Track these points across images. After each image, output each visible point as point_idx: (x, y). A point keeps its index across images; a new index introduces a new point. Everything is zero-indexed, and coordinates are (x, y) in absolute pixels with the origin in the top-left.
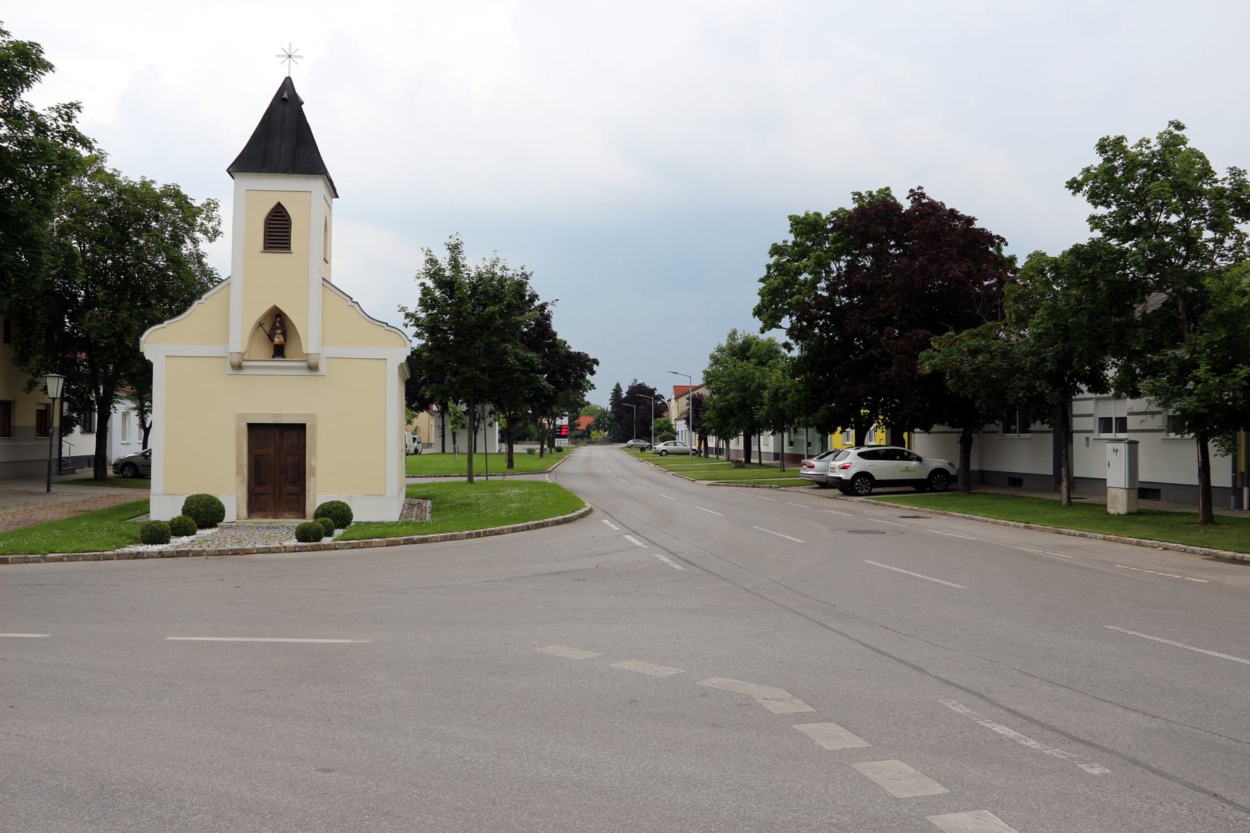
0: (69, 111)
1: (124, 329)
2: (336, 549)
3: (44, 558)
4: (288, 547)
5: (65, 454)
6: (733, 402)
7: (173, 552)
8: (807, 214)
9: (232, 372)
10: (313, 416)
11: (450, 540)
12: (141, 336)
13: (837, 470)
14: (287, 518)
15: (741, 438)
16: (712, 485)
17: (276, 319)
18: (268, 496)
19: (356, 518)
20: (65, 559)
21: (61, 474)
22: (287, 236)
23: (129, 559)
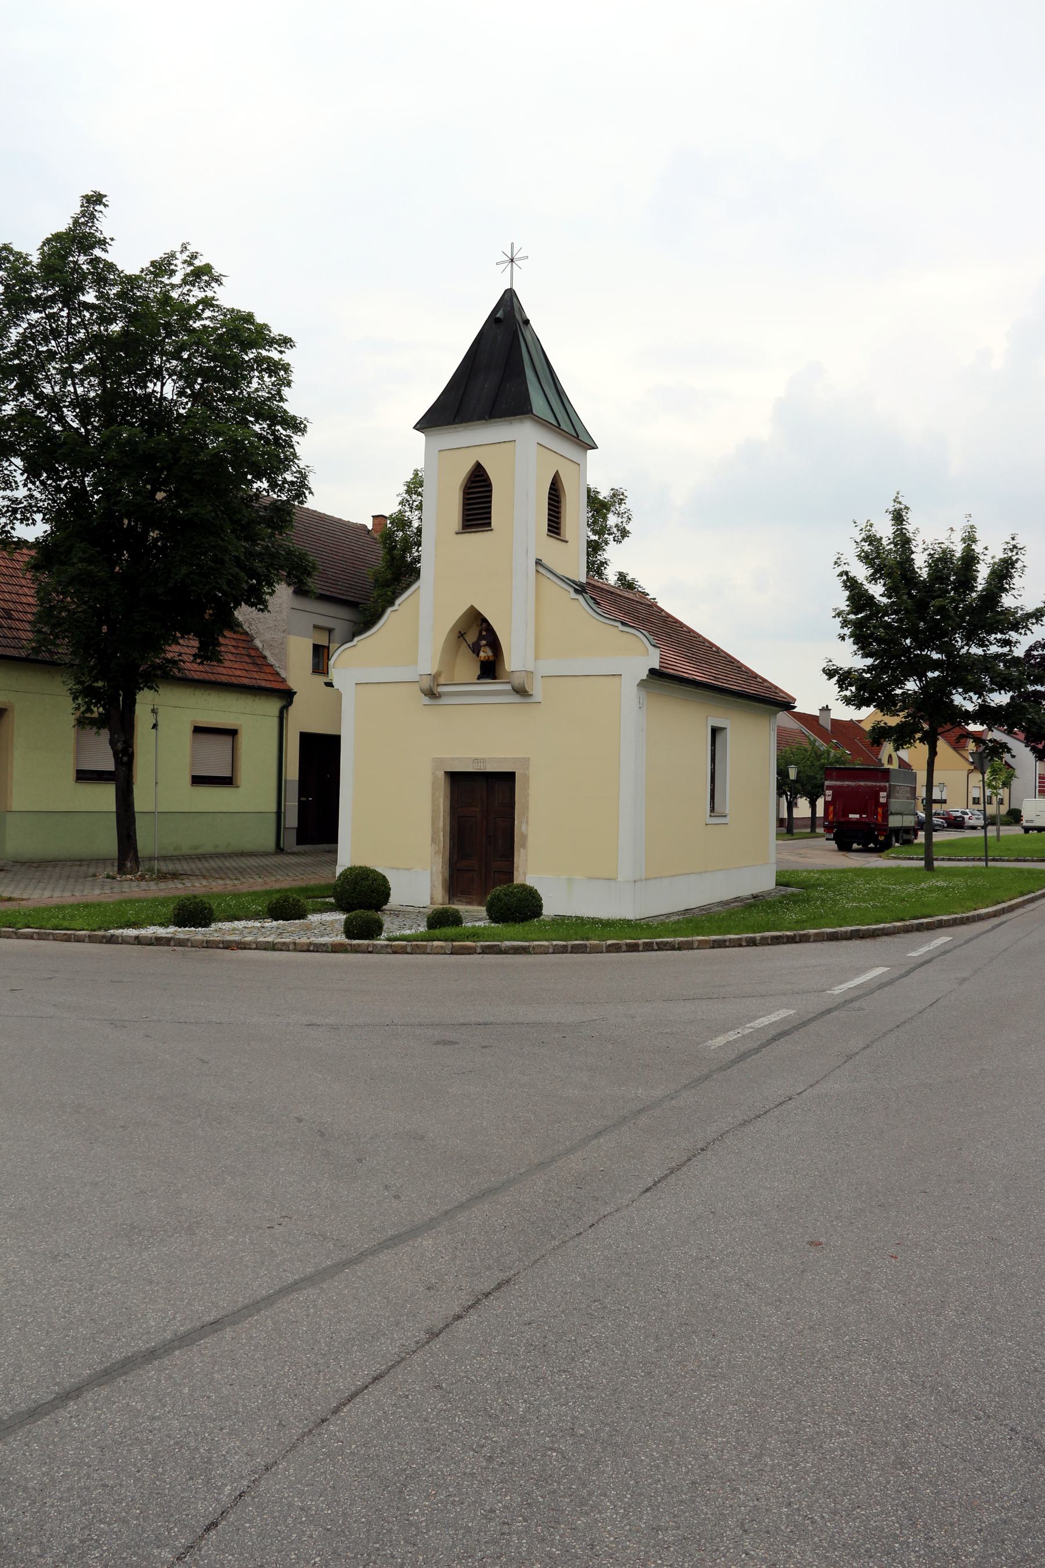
2: (310, 951)
3: (16, 933)
4: (299, 944)
7: (151, 938)
10: (526, 761)
11: (571, 952)
19: (549, 910)
20: (35, 936)
22: (468, 510)
23: (101, 942)
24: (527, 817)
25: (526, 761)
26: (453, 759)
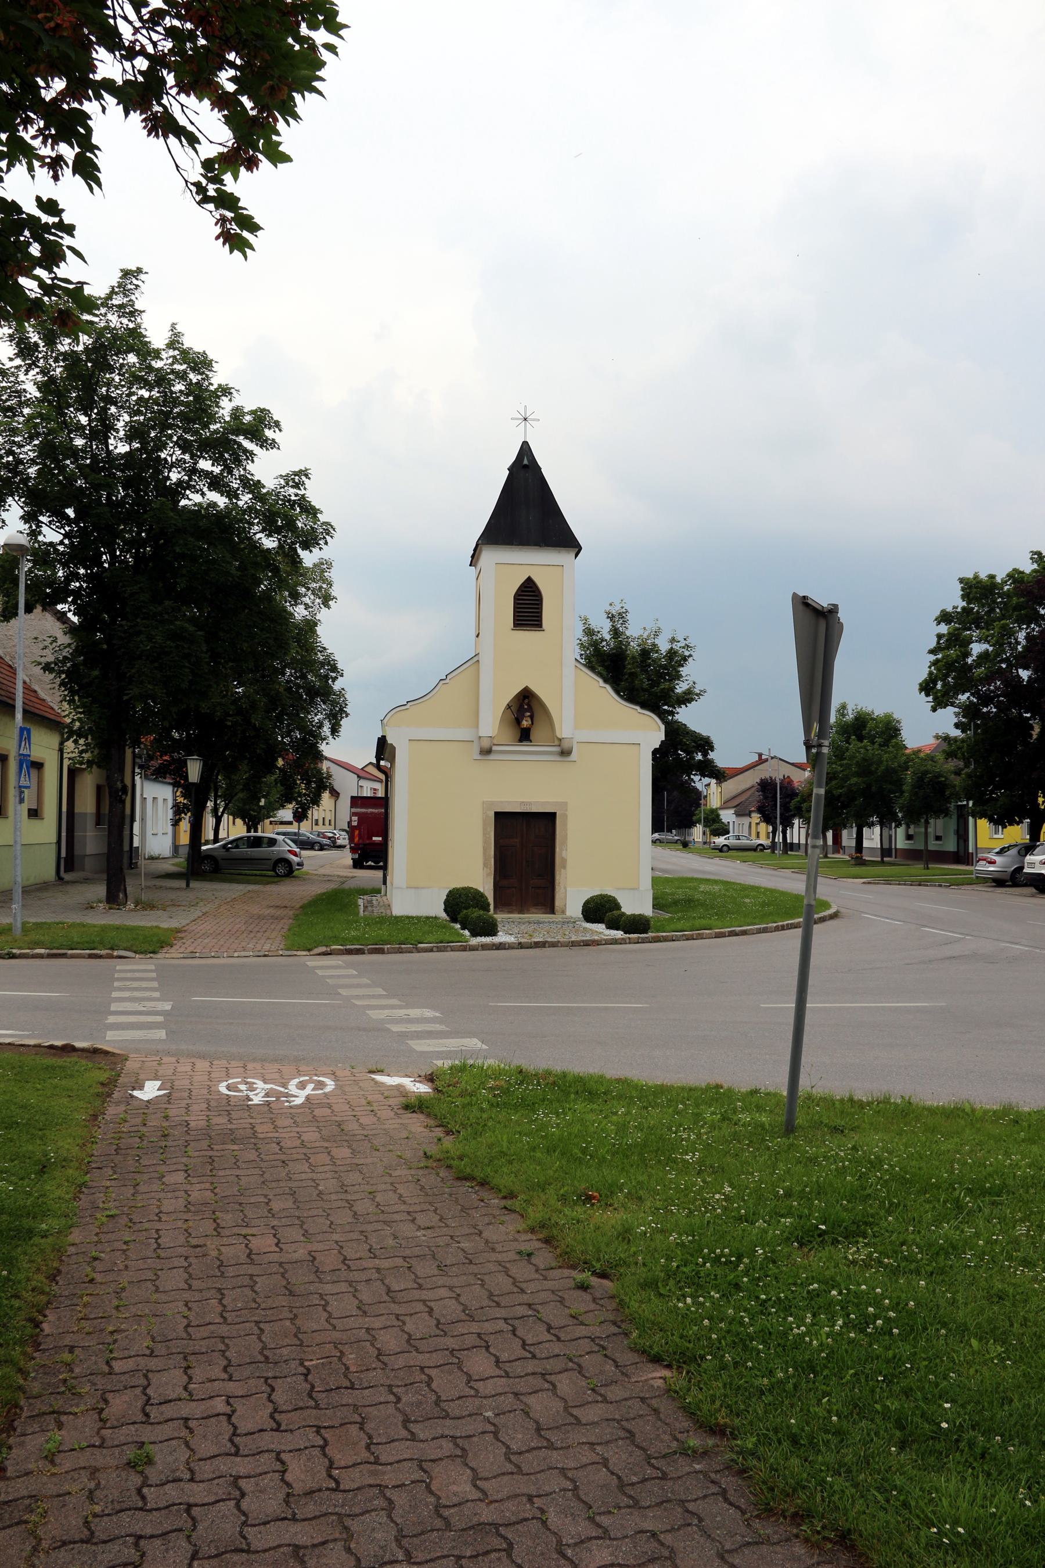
0: (297, 478)
6: (854, 789)
8: (976, 577)
9: (479, 757)
10: (566, 804)
13: (1037, 865)
15: (855, 830)
16: (869, 883)
25: (566, 804)
26: (502, 802)
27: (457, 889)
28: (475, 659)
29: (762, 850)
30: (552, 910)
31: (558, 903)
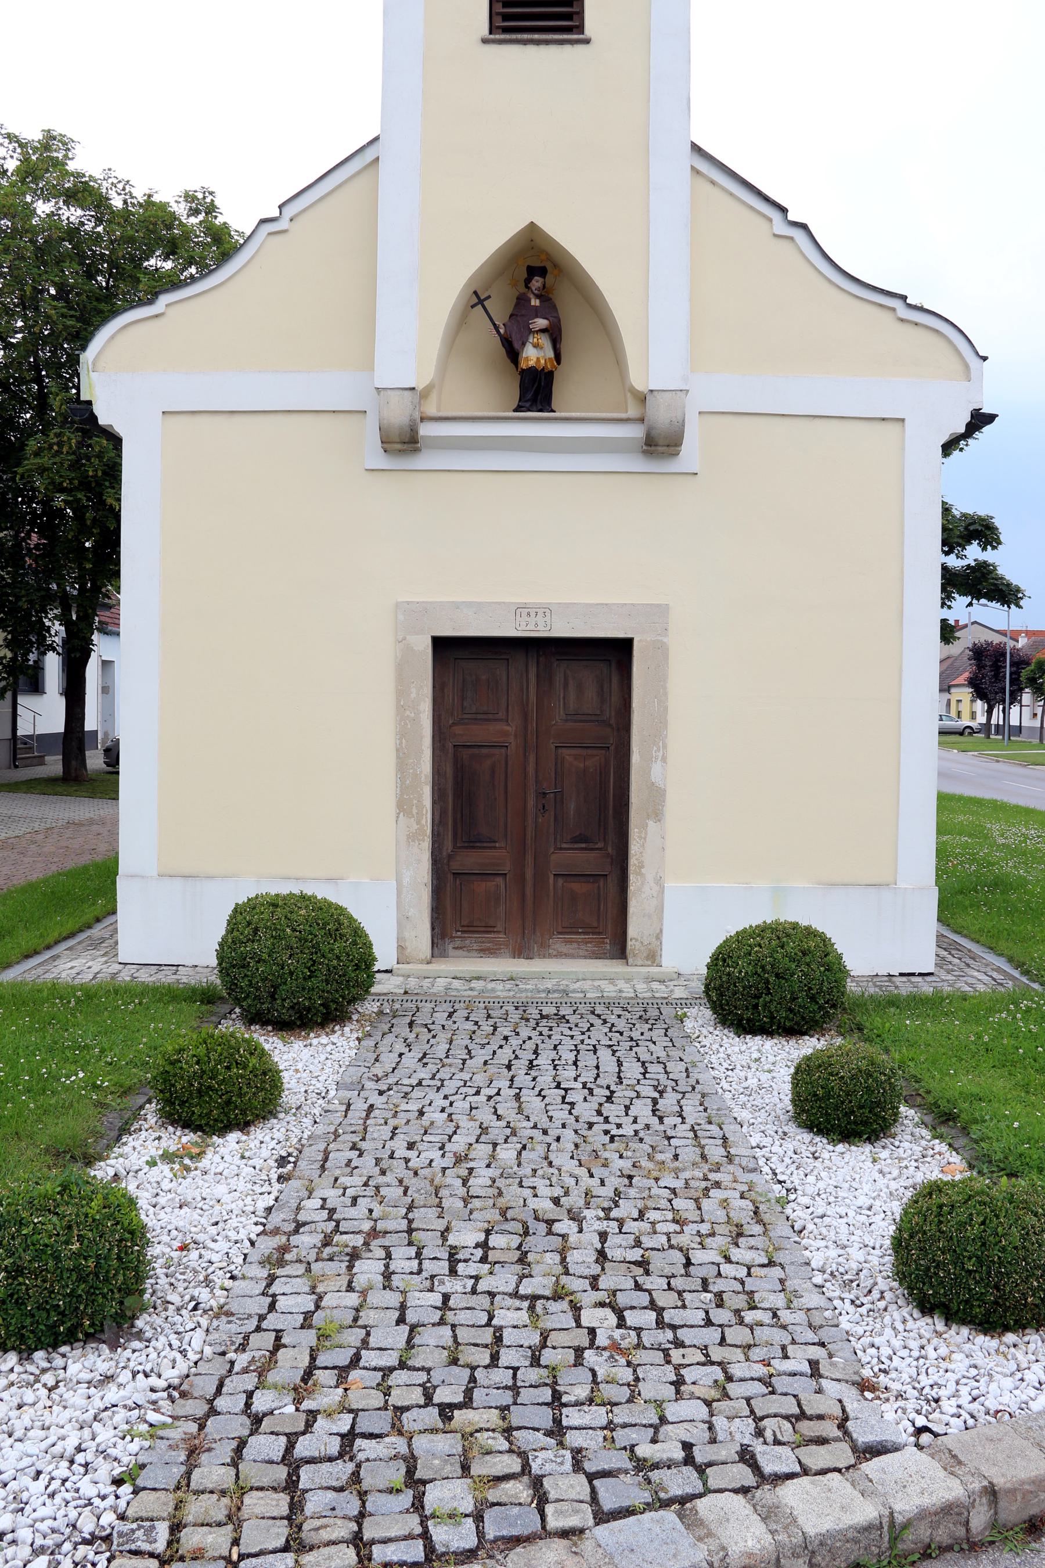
1: (104, 473)
5: (24, 729)
9: (379, 460)
10: (661, 611)
12: (84, 348)
14: (560, 955)
17: (527, 282)
18: (500, 880)
21: (16, 767)
24: (665, 747)
25: (661, 611)
26: (457, 606)
27: (274, 903)
28: (369, 156)
29: (970, 734)
30: (620, 950)
31: (634, 929)
